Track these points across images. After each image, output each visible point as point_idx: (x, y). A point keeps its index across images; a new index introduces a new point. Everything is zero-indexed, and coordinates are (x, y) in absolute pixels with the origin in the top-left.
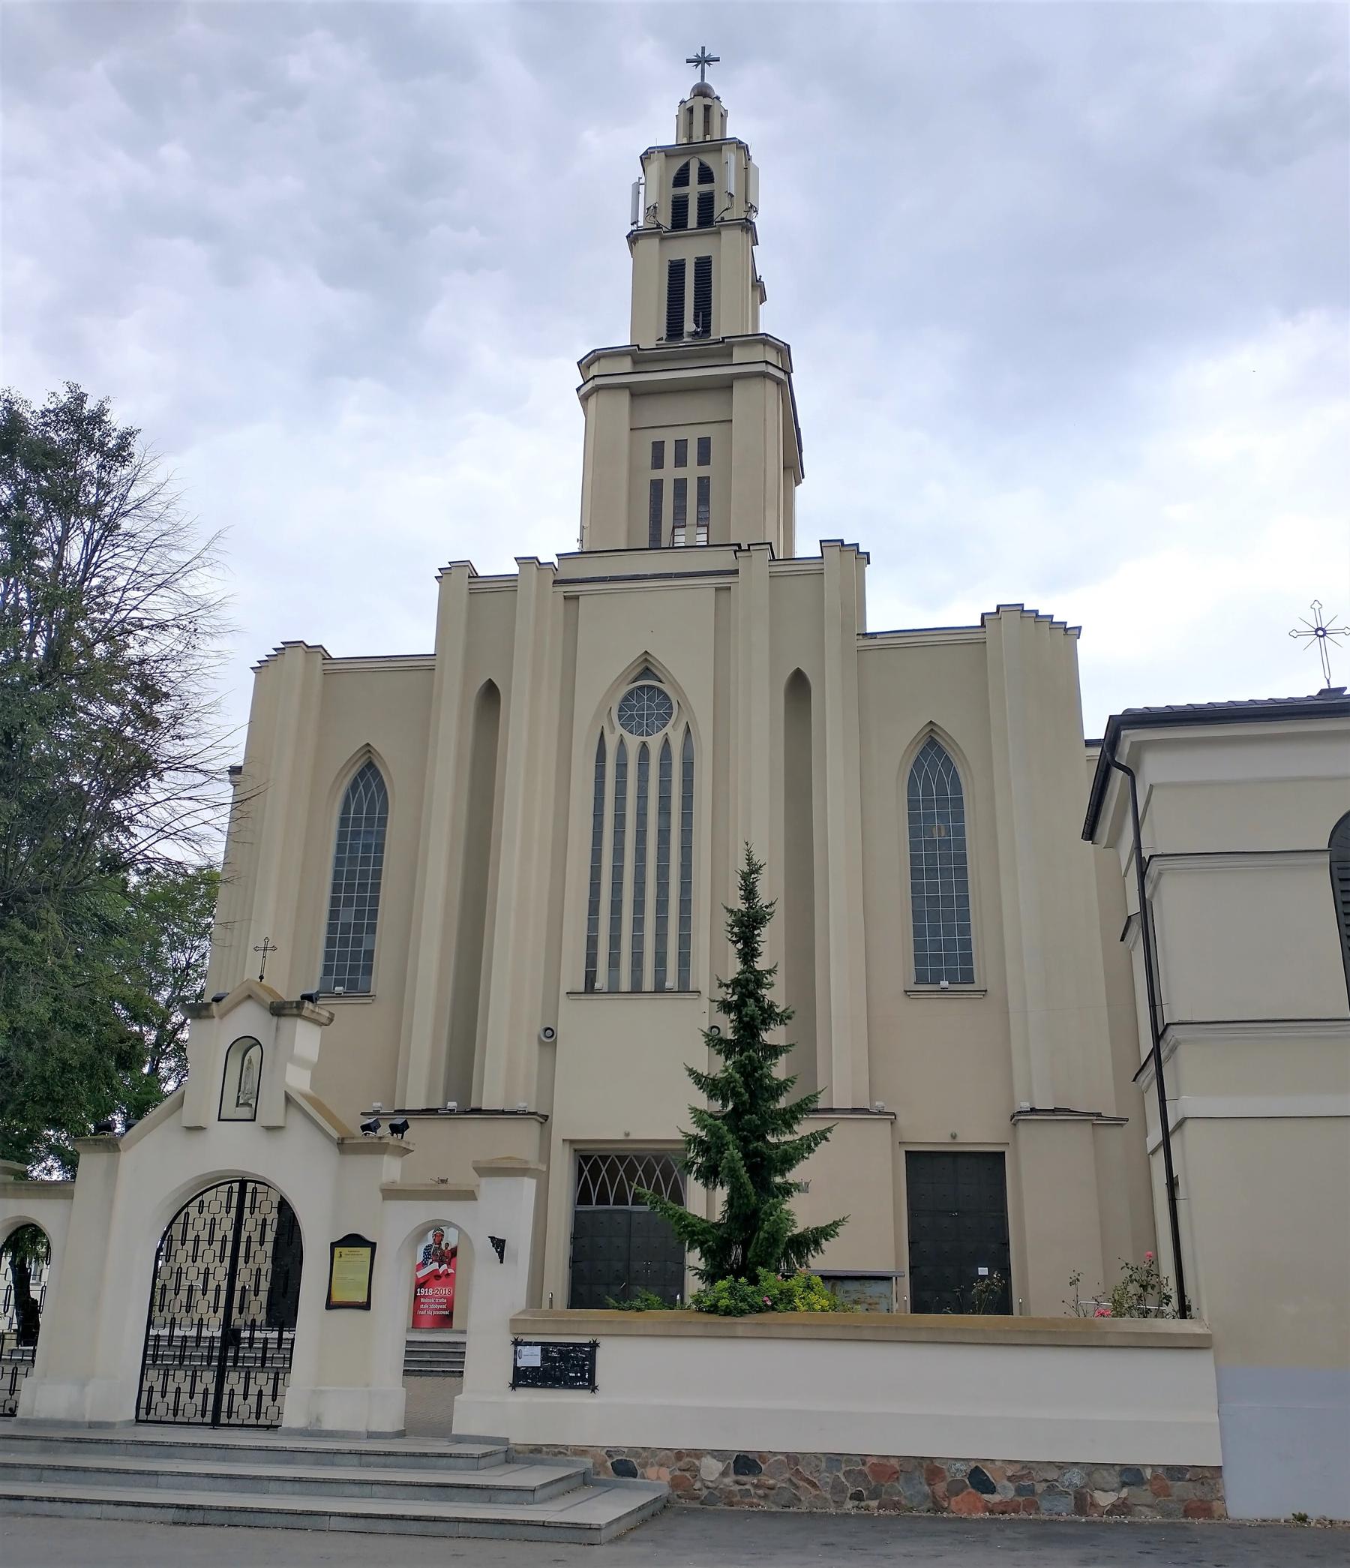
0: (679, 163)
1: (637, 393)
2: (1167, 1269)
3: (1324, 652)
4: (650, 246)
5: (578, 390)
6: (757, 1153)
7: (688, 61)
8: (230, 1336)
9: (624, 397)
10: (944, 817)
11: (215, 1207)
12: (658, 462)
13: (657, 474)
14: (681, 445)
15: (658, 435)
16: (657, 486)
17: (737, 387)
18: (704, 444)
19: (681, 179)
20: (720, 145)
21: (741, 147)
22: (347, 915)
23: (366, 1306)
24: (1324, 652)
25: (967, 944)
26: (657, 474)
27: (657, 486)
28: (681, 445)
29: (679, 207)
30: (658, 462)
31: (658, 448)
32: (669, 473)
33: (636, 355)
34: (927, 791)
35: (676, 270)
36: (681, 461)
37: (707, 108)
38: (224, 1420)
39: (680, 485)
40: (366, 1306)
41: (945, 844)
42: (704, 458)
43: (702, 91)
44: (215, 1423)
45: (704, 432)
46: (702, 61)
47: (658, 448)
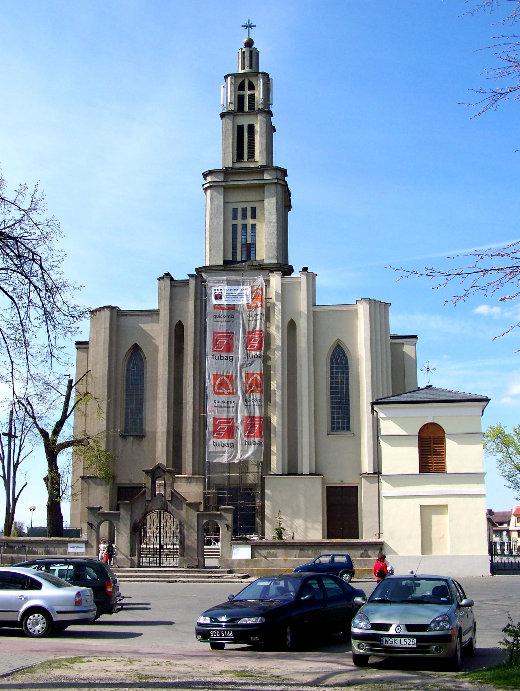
0: (240, 81)
1: (227, 189)
2: (403, 398)
3: (428, 374)
4: (228, 120)
5: (203, 185)
6: (513, 683)
7: (243, 26)
8: (161, 547)
9: (222, 190)
10: (342, 372)
11: (154, 517)
12: (235, 217)
13: (235, 222)
14: (244, 210)
15: (235, 206)
16: (235, 227)
17: (266, 188)
18: (253, 210)
19: (241, 87)
20: (257, 74)
21: (266, 75)
22: (133, 406)
23: (168, 274)
24: (428, 374)
25: (348, 418)
26: (235, 222)
27: (235, 227)
28: (244, 210)
29: (241, 100)
30: (235, 217)
31: (235, 210)
32: (240, 222)
33: (227, 172)
34: (337, 364)
35: (240, 129)
36: (244, 217)
37: (251, 52)
38: (161, 565)
39: (244, 227)
40: (168, 274)
41: (342, 382)
42: (253, 216)
43: (249, 43)
44: (160, 566)
45: (253, 205)
46: (249, 26)
47: (235, 210)
